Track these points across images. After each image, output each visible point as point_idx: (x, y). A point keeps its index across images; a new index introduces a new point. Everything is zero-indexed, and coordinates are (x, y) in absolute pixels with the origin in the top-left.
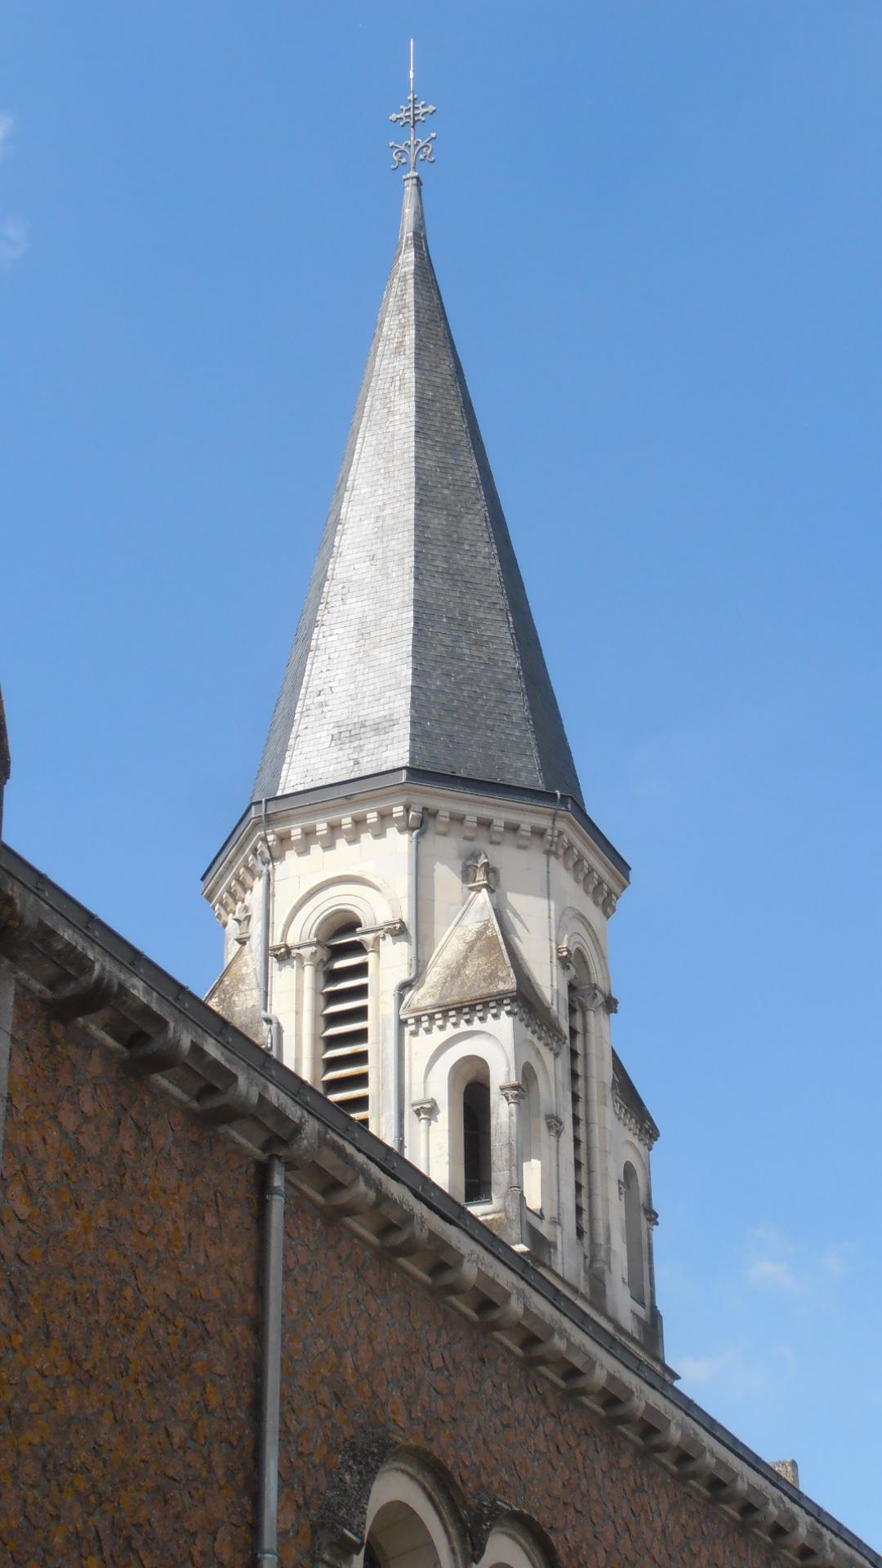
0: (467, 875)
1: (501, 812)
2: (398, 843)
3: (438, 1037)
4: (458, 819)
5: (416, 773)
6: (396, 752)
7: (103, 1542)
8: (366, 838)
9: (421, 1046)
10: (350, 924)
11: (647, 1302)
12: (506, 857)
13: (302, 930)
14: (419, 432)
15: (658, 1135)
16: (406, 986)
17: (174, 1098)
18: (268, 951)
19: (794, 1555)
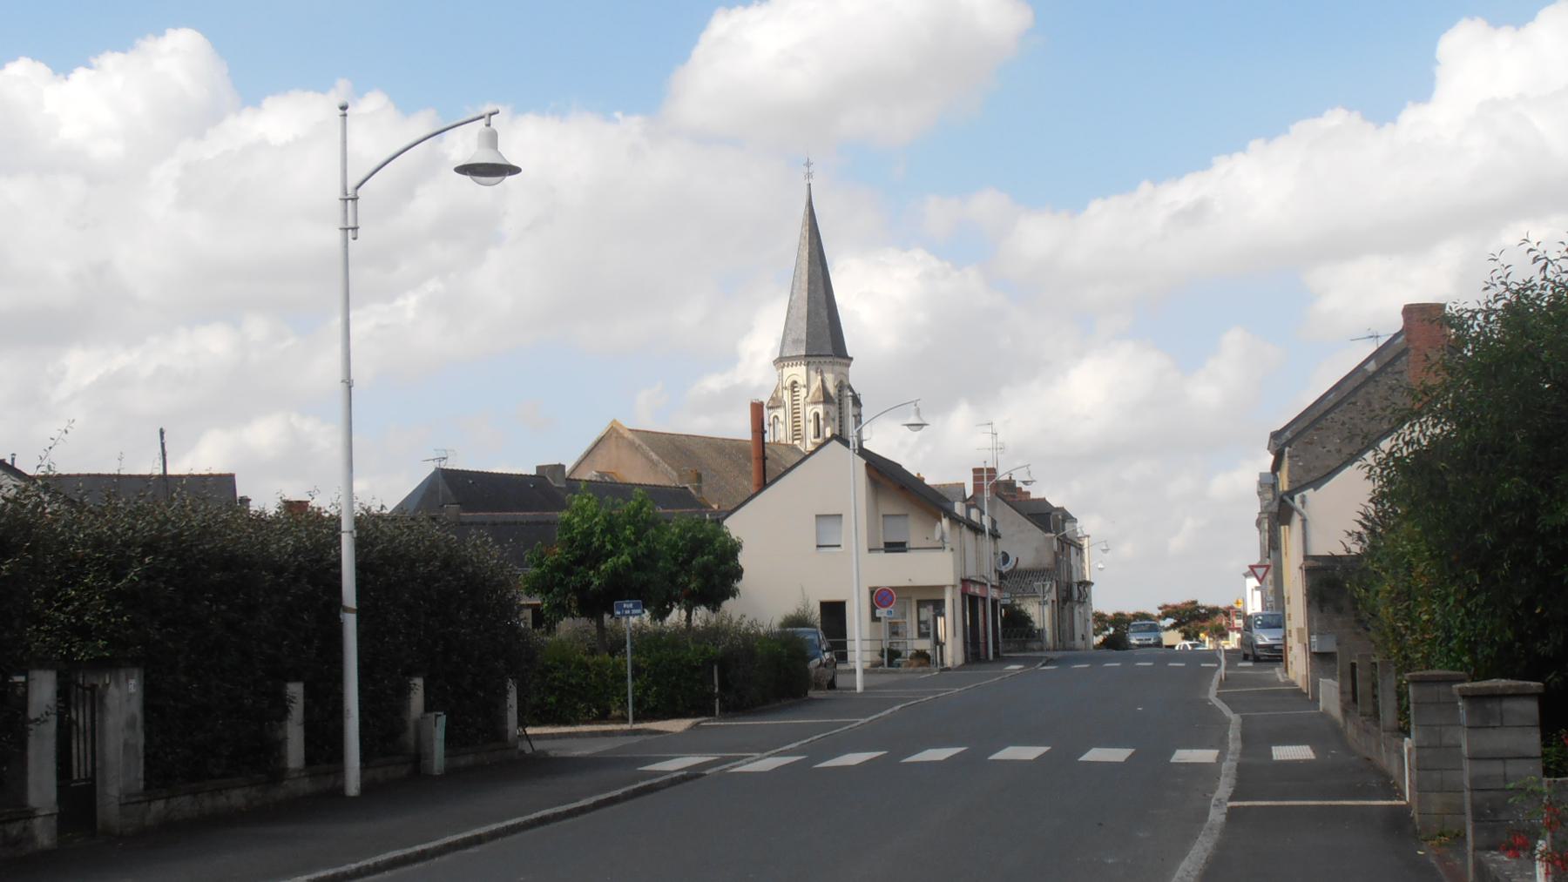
0: (817, 372)
1: (822, 360)
2: (804, 368)
3: (811, 407)
4: (814, 362)
5: (806, 356)
6: (804, 353)
7: (704, 483)
8: (798, 366)
9: (809, 408)
10: (795, 382)
11: (853, 440)
12: (825, 368)
13: (788, 384)
14: (809, 262)
15: (742, 571)
16: (805, 398)
17: (1016, 670)
18: (783, 388)
19: (1336, 664)
